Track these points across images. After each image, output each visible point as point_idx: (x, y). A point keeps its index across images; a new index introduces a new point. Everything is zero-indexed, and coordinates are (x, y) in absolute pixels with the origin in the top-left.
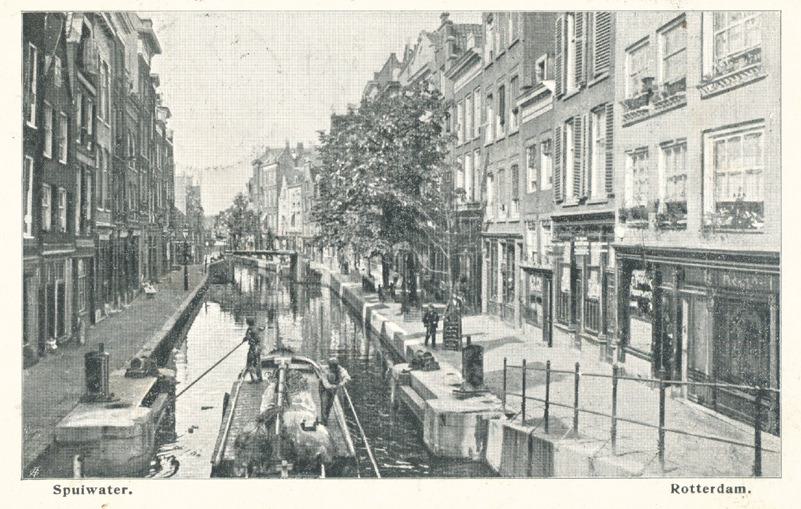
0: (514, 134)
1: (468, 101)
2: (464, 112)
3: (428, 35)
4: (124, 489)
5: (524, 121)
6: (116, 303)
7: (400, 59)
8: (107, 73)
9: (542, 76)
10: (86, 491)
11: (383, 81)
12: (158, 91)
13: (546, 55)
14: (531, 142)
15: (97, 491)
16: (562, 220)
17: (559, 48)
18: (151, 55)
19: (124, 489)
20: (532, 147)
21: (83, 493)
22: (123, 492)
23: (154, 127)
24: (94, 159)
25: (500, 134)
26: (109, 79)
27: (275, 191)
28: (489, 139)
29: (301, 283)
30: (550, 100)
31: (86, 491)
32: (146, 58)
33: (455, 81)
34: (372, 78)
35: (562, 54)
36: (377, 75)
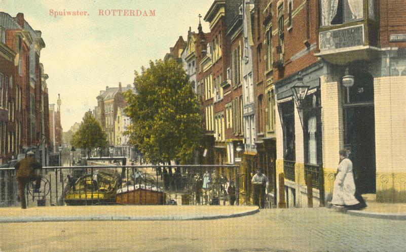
4: (85, 12)
21: (65, 15)
22: (85, 15)
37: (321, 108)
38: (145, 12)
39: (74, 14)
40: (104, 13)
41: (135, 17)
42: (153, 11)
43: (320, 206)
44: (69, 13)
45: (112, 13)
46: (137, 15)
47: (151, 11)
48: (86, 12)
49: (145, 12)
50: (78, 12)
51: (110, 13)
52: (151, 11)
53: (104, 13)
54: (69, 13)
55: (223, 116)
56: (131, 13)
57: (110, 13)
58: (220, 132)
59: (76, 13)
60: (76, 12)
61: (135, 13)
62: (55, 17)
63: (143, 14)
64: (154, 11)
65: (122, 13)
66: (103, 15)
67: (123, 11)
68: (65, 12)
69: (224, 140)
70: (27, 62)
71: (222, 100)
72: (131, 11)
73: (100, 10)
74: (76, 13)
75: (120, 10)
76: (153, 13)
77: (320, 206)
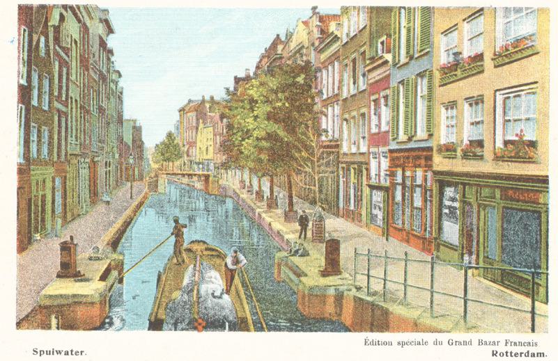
7: (283, 39)
10: (55, 352)
12: (113, 59)
14: (373, 98)
15: (63, 353)
19: (82, 352)
28: (345, 95)
31: (55, 352)
34: (264, 52)
44: (59, 352)
54: (59, 352)
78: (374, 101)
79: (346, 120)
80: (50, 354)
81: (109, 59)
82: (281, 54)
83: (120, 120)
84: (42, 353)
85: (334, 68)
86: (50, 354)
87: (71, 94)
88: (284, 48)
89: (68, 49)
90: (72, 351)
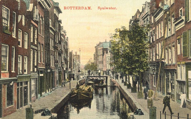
0: (170, 65)
1: (157, 44)
2: (158, 28)
3: (148, 3)
4: (115, 8)
5: (176, 30)
6: (46, 92)
7: (141, 11)
8: (43, 20)
9: (181, 15)
10: (106, 8)
11: (134, 19)
12: (61, 25)
13: (182, 8)
14: (178, 38)
15: (108, 8)
16: (188, 64)
17: (186, 5)
18: (59, 13)
19: (115, 8)
20: (179, 39)
21: (105, 9)
22: (115, 9)
23: (61, 37)
24: (38, 47)
25: (169, 35)
26: (43, 22)
27: (102, 56)
28: (166, 37)
29: (109, 86)
30: (184, 22)
31: (106, 8)
32: (57, 15)
33: (156, 17)
34: (131, 18)
35: (187, 7)
36: (133, 17)
37: (123, 33)
38: (86, 8)
39: (110, 8)
40: (66, 8)
41: (81, 10)
42: (89, 7)
43: (127, 89)
44: (107, 8)
45: (70, 8)
46: (82, 9)
47: (88, 7)
48: (115, 8)
49: (86, 8)
50: (111, 8)
51: (67, 8)
52: (88, 7)
53: (66, 8)
54: (107, 8)
55: (174, 46)
56: (79, 8)
57: (67, 8)
58: (170, 58)
59: (111, 8)
60: (111, 7)
61: (81, 8)
62: (101, 10)
63: (84, 9)
64: (90, 7)
65: (75, 8)
66: (80, 9)
67: (76, 7)
68: (105, 8)
69: (174, 62)
70: (187, 75)
71: (160, 38)
72: (79, 7)
73: (64, 7)
74: (111, 8)
75: (74, 7)
76: (89, 8)
77: (127, 89)
78: (178, 39)
79: (167, 49)
80: (104, 9)
81: (59, 25)
82: (139, 19)
83: (66, 50)
84: (101, 8)
85: (161, 24)
86: (104, 9)
87: (39, 40)
88: (140, 16)
89: (38, 21)
90: (111, 8)
